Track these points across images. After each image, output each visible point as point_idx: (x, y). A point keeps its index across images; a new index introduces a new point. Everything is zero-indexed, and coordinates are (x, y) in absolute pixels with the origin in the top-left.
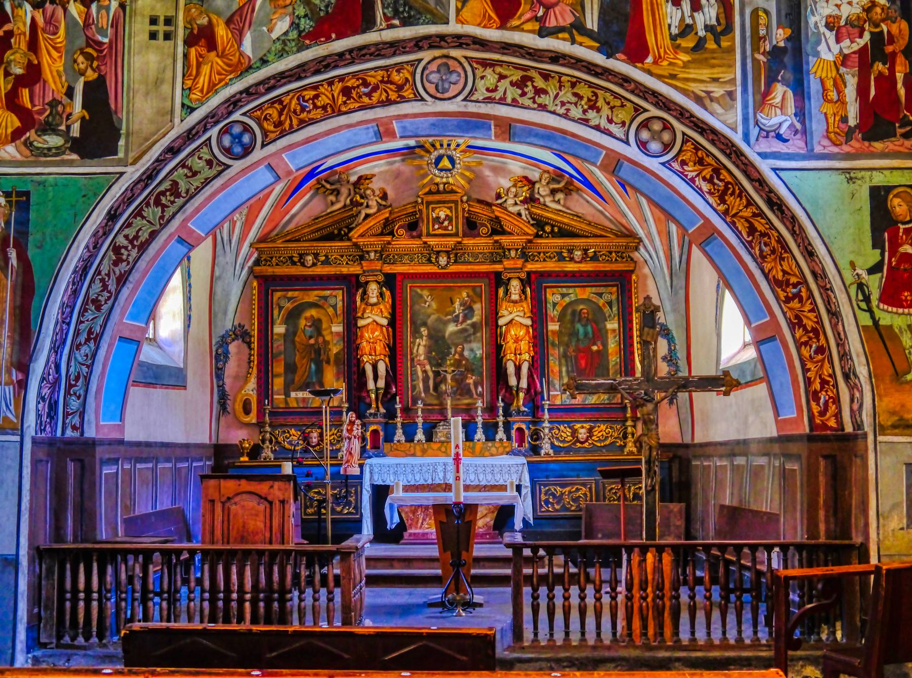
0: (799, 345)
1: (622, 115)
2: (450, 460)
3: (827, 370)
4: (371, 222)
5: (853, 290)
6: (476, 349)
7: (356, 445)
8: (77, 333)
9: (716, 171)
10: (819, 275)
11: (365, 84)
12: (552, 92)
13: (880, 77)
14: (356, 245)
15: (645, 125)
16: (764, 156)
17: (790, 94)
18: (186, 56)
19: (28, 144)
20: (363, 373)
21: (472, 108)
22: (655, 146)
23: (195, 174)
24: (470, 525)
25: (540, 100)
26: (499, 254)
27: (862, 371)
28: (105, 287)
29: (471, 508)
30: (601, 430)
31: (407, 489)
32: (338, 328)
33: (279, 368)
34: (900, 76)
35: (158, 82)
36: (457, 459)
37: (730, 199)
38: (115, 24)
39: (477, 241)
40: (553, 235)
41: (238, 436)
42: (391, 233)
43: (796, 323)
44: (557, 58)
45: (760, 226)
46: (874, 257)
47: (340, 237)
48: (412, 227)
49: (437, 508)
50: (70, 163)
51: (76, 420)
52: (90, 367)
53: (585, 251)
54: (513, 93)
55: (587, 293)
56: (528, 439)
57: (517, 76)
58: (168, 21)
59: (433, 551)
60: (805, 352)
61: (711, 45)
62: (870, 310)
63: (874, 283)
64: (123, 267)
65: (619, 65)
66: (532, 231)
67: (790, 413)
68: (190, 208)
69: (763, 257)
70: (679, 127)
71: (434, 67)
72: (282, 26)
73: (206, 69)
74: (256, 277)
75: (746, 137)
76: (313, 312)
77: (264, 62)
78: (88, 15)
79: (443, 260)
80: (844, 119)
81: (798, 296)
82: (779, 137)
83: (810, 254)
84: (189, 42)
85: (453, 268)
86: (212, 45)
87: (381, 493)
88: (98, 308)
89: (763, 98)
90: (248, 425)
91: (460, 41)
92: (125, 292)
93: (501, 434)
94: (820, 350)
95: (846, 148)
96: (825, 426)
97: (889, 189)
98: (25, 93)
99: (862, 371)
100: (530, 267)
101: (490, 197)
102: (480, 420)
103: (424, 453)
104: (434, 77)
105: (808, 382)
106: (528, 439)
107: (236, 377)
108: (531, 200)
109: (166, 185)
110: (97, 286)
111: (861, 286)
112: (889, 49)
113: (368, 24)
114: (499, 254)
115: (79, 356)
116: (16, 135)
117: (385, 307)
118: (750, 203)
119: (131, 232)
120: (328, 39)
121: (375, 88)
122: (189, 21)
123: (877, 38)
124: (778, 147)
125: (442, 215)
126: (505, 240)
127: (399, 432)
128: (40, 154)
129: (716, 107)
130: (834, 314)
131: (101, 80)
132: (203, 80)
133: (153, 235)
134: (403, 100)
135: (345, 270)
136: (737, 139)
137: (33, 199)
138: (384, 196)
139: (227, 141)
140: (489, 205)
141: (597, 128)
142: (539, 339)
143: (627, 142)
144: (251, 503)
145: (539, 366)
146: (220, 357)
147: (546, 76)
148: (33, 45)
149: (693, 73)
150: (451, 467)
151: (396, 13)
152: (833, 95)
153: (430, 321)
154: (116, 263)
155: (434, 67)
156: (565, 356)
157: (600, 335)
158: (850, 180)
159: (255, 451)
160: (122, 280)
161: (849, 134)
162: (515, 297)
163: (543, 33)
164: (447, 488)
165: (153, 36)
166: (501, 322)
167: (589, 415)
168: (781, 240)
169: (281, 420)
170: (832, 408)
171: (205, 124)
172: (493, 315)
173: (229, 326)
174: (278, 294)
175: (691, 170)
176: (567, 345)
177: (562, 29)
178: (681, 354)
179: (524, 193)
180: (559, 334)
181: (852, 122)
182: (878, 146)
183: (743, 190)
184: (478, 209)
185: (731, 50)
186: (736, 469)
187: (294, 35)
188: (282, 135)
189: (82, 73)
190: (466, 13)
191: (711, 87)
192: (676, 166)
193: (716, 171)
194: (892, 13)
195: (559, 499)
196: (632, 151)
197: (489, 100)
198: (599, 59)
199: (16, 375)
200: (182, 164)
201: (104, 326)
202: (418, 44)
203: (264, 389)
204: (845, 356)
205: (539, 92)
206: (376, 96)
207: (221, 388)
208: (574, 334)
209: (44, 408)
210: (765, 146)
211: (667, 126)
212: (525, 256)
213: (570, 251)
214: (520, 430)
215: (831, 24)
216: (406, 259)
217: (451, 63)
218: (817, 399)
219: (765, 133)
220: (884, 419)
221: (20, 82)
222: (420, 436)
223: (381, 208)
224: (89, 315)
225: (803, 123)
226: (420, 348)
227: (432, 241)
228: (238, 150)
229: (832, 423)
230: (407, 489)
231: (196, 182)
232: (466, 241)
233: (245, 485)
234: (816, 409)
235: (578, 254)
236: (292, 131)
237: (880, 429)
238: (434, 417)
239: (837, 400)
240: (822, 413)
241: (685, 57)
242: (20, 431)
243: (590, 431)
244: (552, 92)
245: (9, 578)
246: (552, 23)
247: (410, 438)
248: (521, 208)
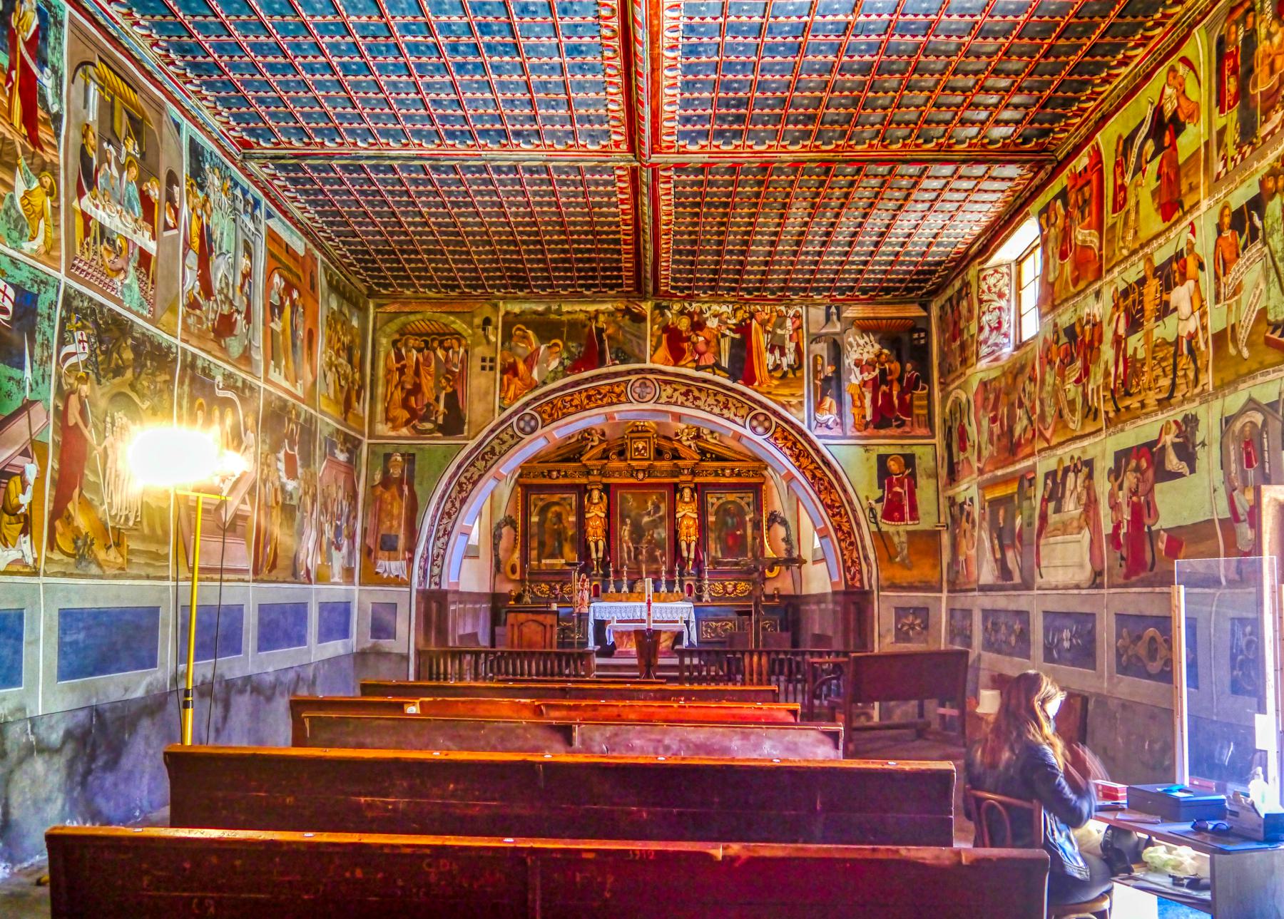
0: (839, 541)
1: (742, 412)
2: (645, 604)
3: (855, 555)
4: (594, 451)
5: (867, 512)
6: (662, 533)
7: (586, 594)
8: (438, 531)
9: (794, 444)
10: (850, 503)
11: (599, 393)
12: (703, 399)
13: (884, 394)
14: (585, 465)
15: (755, 417)
16: (819, 437)
17: (834, 403)
18: (501, 380)
19: (414, 427)
20: (588, 548)
21: (659, 407)
22: (760, 430)
23: (504, 442)
24: (657, 643)
25: (698, 403)
26: (677, 472)
27: (872, 556)
28: (453, 505)
29: (657, 633)
30: (742, 586)
31: (618, 621)
32: (572, 519)
33: (535, 544)
34: (895, 393)
35: (487, 393)
36: (649, 603)
37: (802, 459)
38: (462, 362)
39: (665, 463)
40: (712, 460)
41: (507, 588)
42: (607, 458)
43: (838, 528)
44: (705, 381)
45: (818, 473)
46: (879, 493)
47: (574, 460)
48: (621, 454)
49: (636, 632)
50: (438, 438)
51: (437, 580)
52: (445, 550)
53: (733, 470)
54: (681, 399)
55: (731, 497)
56: (695, 591)
57: (683, 389)
58: (492, 360)
59: (635, 662)
60: (843, 545)
61: (790, 375)
62: (876, 523)
63: (879, 509)
64: (464, 494)
65: (740, 386)
66: (698, 457)
67: (836, 579)
68: (501, 461)
69: (820, 492)
70: (774, 419)
71: (637, 384)
72: (554, 364)
73: (512, 388)
74: (521, 485)
75: (809, 427)
76: (556, 508)
77: (544, 383)
78: (447, 357)
79: (641, 475)
80: (864, 417)
81: (839, 513)
82: (827, 427)
83: (845, 491)
84: (503, 372)
85: (647, 481)
86: (516, 374)
87: (600, 625)
88: (450, 517)
89: (819, 406)
90: (514, 581)
91: (652, 371)
92: (465, 508)
93: (677, 588)
94: (851, 544)
95: (865, 433)
96: (853, 586)
97: (888, 456)
98: (413, 399)
99: (872, 556)
100: (697, 480)
101: (671, 435)
102: (663, 579)
103: (628, 600)
104: (638, 390)
105: (845, 562)
106: (695, 591)
107: (506, 550)
108: (698, 437)
109: (488, 449)
110: (449, 505)
111: (871, 509)
112: (889, 378)
113: (602, 363)
114: (677, 472)
115: (439, 544)
116: (407, 423)
117: (603, 505)
118: (813, 461)
119: (468, 475)
120: (580, 371)
121: (605, 396)
122: (503, 359)
123: (883, 372)
124: (828, 432)
125: (641, 447)
126: (680, 463)
127: (612, 586)
128: (420, 433)
129: (793, 410)
130: (858, 524)
131: (455, 392)
132: (511, 394)
133: (481, 476)
134: (620, 402)
135: (577, 481)
136: (804, 427)
137: (417, 458)
138: (603, 434)
139: (522, 424)
140: (670, 439)
141: (728, 419)
142: (702, 528)
143: (744, 427)
144: (534, 626)
145: (702, 544)
146: (496, 537)
147: (700, 390)
148: (417, 373)
149: (781, 391)
150: (645, 609)
151: (617, 358)
152: (858, 403)
153: (633, 514)
154: (460, 492)
155: (637, 384)
156: (719, 538)
157: (742, 524)
158: (867, 451)
159: (519, 598)
160: (463, 501)
161: (866, 426)
162: (687, 500)
163: (698, 368)
164: (643, 621)
165: (483, 368)
166: (678, 515)
167: (735, 576)
168: (830, 482)
169: (535, 577)
170: (858, 576)
171: (510, 417)
172: (673, 511)
173: (502, 516)
174: (533, 497)
175: (780, 443)
176: (720, 531)
177: (708, 367)
178: (794, 538)
179: (694, 433)
180: (715, 523)
181: (869, 418)
182: (882, 432)
183: (809, 454)
184: (663, 442)
185: (802, 378)
186: (821, 610)
187: (561, 368)
188: (553, 421)
189: (444, 388)
190: (656, 357)
191: (790, 399)
192: (772, 440)
193: (794, 444)
194: (892, 358)
195: (715, 630)
196: (747, 432)
197: (668, 403)
198: (728, 383)
199: (407, 555)
200: (497, 437)
201: (453, 527)
202: (629, 373)
203: (525, 558)
204: (864, 548)
205: (696, 398)
206: (605, 400)
207: (497, 556)
208: (725, 523)
209: (421, 572)
210: (820, 432)
211: (767, 418)
212: (693, 473)
213: (723, 470)
214: (689, 586)
215: (858, 363)
216: (617, 474)
217: (648, 383)
218: (849, 571)
219: (820, 424)
220: (883, 582)
221: (410, 393)
222: (625, 589)
223: (601, 441)
224: (445, 521)
225: (841, 418)
226: (625, 532)
227: (634, 463)
228: (528, 429)
229: (858, 584)
230: (618, 621)
231: (505, 447)
232: (656, 463)
233: (531, 616)
234: (849, 577)
235: (728, 472)
236: (558, 419)
237: (880, 588)
238: (636, 577)
239: (860, 572)
240: (853, 579)
241: (776, 382)
242: (408, 584)
243: (735, 586)
244: (703, 399)
245: (405, 665)
246: (702, 363)
247: (618, 591)
248: (692, 443)
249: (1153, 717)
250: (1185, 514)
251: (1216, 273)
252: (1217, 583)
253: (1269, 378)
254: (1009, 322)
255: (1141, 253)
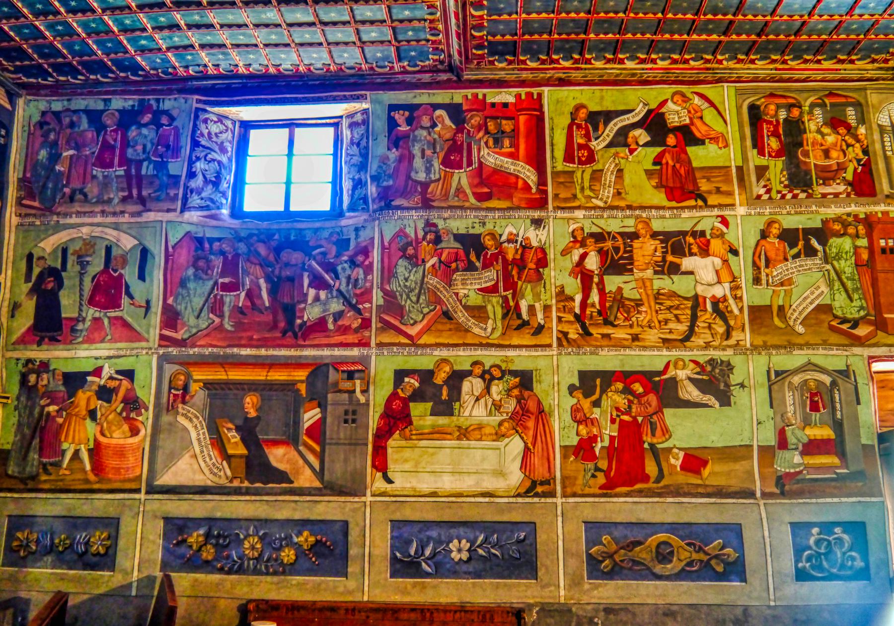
165: (354, 421)
249: (665, 614)
250: (714, 438)
251: (754, 264)
252: (751, 494)
253: (831, 352)
254: (228, 182)
255: (637, 212)
